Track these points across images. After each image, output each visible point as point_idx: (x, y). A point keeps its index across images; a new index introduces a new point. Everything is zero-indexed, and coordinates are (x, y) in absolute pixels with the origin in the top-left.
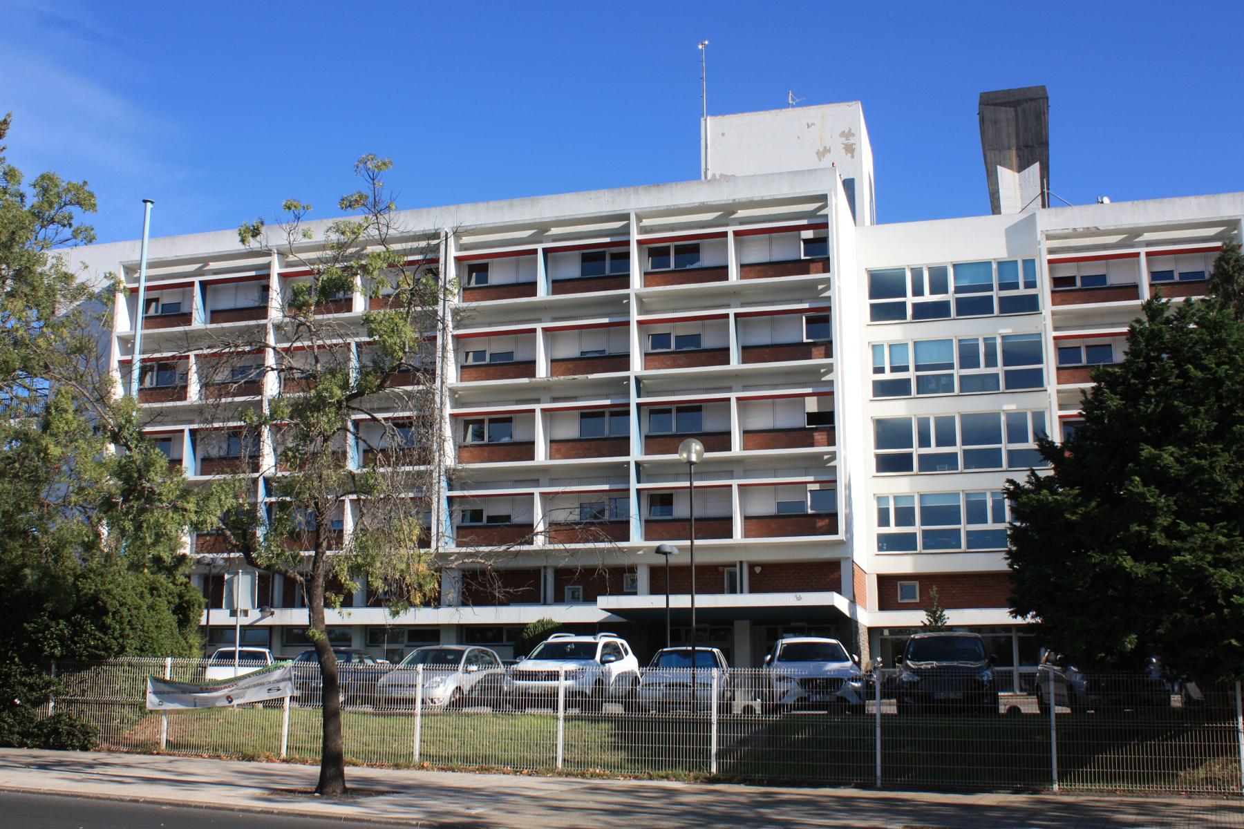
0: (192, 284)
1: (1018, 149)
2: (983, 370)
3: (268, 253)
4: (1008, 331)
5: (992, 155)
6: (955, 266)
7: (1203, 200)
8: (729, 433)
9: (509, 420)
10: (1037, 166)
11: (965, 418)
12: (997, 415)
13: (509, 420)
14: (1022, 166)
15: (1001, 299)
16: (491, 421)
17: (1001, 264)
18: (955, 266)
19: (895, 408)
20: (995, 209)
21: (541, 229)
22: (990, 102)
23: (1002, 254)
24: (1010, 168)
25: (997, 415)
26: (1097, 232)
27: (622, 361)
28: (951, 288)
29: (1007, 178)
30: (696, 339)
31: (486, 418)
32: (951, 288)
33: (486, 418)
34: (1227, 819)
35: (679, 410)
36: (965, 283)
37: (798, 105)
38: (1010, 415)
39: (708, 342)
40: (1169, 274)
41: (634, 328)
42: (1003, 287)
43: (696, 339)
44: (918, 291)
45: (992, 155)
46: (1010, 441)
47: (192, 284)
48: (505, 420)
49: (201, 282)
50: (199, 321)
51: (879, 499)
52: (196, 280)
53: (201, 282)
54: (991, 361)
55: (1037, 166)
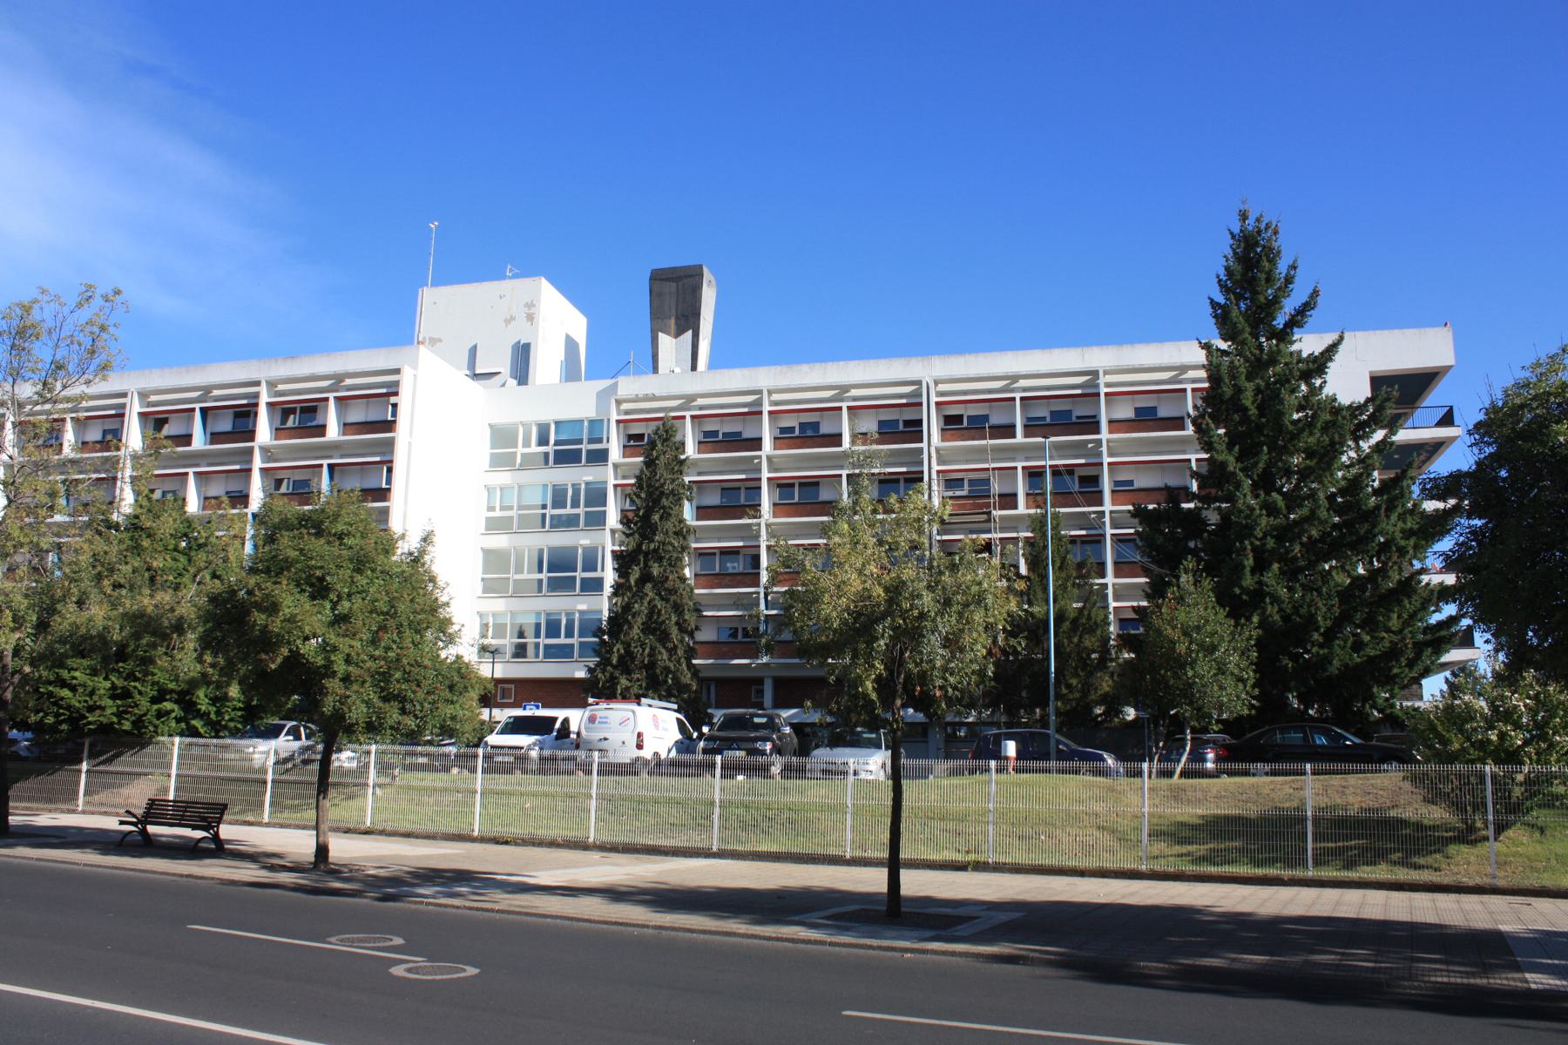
0: (193, 410)
1: (677, 318)
2: (562, 640)
3: (258, 383)
4: (589, 478)
5: (658, 320)
6: (557, 423)
7: (746, 372)
8: (1015, 495)
9: (817, 484)
10: (689, 333)
11: (552, 550)
12: (576, 549)
13: (817, 484)
14: (678, 333)
15: (589, 452)
16: (801, 485)
17: (592, 422)
18: (557, 423)
19: (500, 541)
20: (655, 370)
21: (338, 378)
22: (660, 278)
23: (590, 413)
24: (668, 333)
25: (576, 549)
26: (654, 398)
27: (756, 443)
28: (552, 442)
29: (665, 340)
30: (815, 426)
31: (796, 482)
32: (552, 442)
33: (796, 482)
34: (622, 870)
35: (907, 481)
36: (563, 437)
37: (515, 277)
38: (585, 549)
39: (825, 429)
40: (715, 433)
41: (766, 417)
42: (591, 441)
43: (815, 426)
44: (527, 444)
45: (658, 320)
46: (584, 570)
47: (193, 410)
48: (811, 485)
49: (202, 409)
50: (199, 442)
51: (481, 615)
52: (197, 406)
53: (202, 409)
54: (575, 504)
55: (689, 333)
